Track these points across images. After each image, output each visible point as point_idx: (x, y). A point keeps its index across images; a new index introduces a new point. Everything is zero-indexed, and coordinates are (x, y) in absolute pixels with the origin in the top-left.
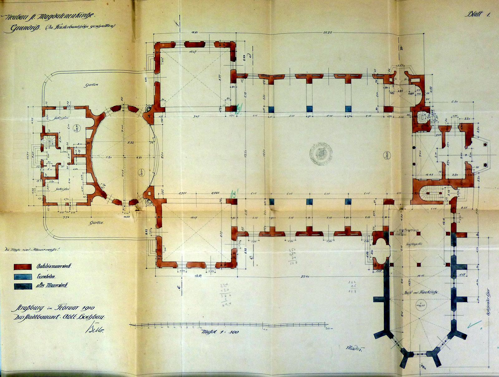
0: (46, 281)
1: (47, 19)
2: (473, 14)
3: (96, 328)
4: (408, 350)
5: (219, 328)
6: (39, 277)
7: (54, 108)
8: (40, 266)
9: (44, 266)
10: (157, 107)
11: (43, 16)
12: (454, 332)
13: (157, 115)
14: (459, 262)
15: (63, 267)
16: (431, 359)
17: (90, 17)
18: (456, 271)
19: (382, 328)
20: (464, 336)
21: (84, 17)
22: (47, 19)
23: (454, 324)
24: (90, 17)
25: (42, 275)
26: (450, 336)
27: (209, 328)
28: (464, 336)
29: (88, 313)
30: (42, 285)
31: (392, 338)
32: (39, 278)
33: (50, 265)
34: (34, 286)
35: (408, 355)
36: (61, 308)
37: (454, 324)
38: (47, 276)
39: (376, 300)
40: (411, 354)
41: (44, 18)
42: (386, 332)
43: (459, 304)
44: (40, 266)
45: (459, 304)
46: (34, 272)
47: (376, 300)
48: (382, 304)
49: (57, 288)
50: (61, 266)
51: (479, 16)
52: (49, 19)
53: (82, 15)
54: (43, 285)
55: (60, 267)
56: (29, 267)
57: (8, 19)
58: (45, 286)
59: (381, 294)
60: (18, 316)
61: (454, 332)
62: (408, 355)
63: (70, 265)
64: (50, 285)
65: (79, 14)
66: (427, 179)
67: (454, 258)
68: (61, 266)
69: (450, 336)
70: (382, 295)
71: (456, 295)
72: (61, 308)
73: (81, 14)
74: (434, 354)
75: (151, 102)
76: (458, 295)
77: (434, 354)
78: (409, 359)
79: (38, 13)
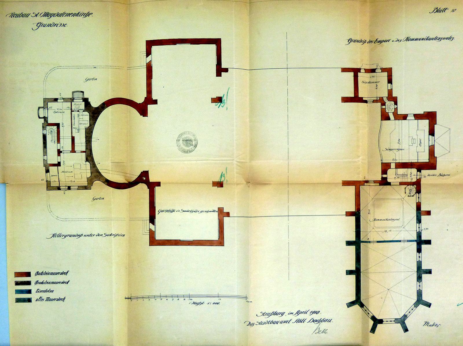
0: (45, 296)
1: (49, 17)
2: (438, 10)
3: (322, 329)
4: (379, 317)
5: (206, 300)
6: (38, 291)
7: (56, 100)
8: (38, 273)
9: (42, 274)
10: (150, 100)
11: (47, 15)
12: (420, 301)
13: (150, 107)
14: (423, 238)
15: (61, 274)
16: (399, 325)
17: (89, 16)
18: (421, 216)
19: (354, 298)
20: (429, 305)
21: (84, 16)
22: (49, 17)
23: (419, 294)
24: (89, 16)
25: (40, 281)
26: (416, 304)
27: (197, 300)
28: (429, 305)
29: (316, 317)
30: (41, 299)
31: (363, 307)
32: (38, 292)
33: (48, 272)
34: (33, 300)
35: (377, 322)
36: (65, 14)
37: (419, 294)
38: (46, 290)
39: (349, 243)
40: (381, 321)
41: (47, 16)
42: (358, 301)
43: (424, 276)
44: (38, 273)
45: (424, 276)
46: (32, 279)
47: (349, 243)
48: (353, 218)
49: (55, 302)
50: (60, 282)
51: (444, 12)
52: (51, 17)
53: (82, 14)
54: (43, 300)
55: (58, 274)
56: (28, 274)
57: (11, 17)
58: (45, 300)
59: (353, 238)
60: (250, 323)
61: (420, 301)
62: (377, 322)
63: (67, 272)
64: (48, 299)
65: (79, 13)
66: (392, 89)
67: (419, 235)
68: (60, 282)
69: (416, 304)
70: (354, 239)
71: (421, 238)
72: (65, 14)
73: (81, 13)
74: (402, 321)
75: (145, 95)
76: (423, 267)
77: (402, 321)
78: (379, 326)
79: (43, 11)
